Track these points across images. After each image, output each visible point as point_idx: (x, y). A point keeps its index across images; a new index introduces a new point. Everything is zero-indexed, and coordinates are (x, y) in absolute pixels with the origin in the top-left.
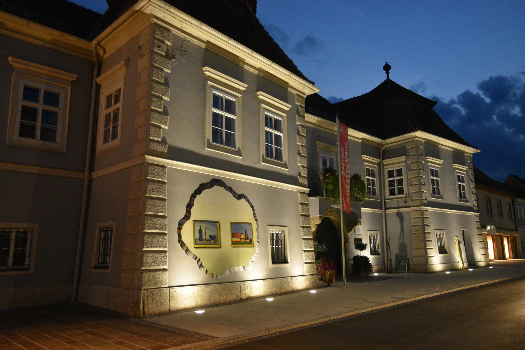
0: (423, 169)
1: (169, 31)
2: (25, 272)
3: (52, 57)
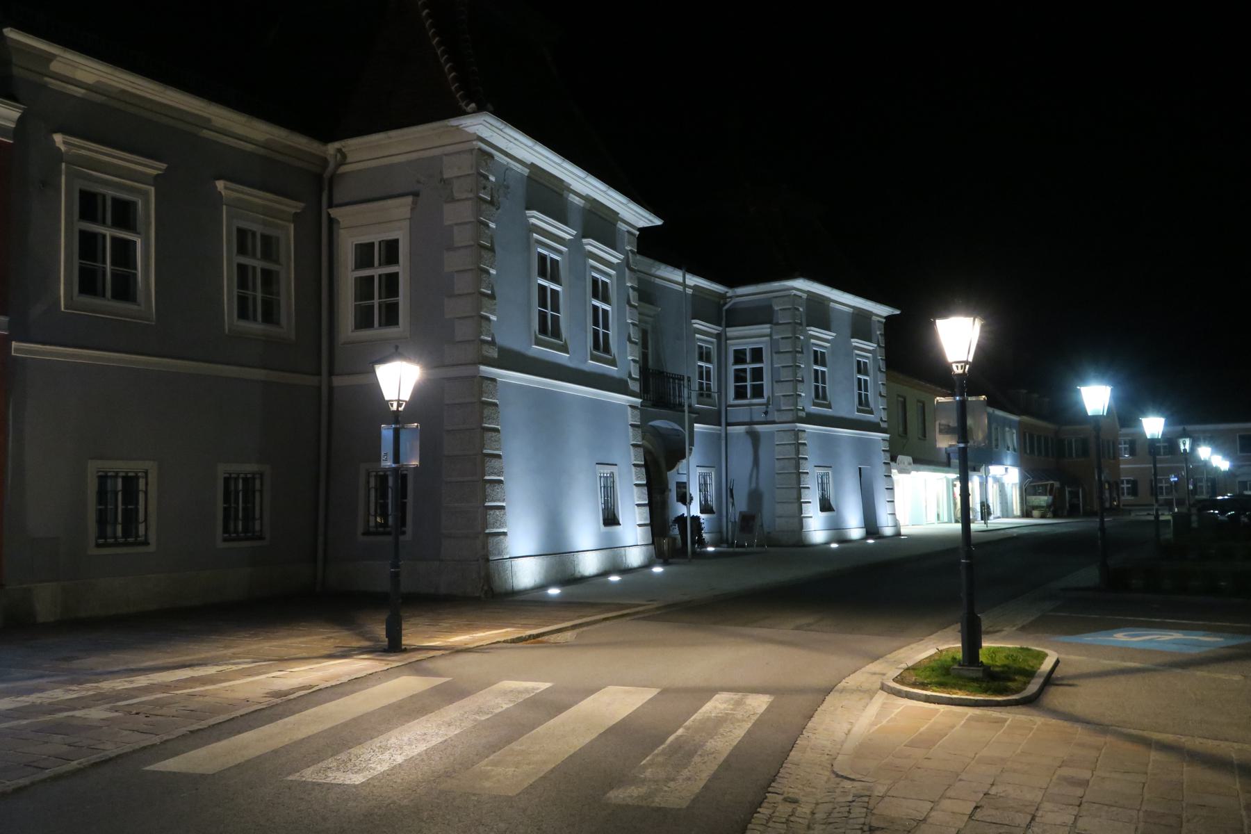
0: (802, 352)
1: (491, 156)
2: (141, 549)
3: (265, 172)
